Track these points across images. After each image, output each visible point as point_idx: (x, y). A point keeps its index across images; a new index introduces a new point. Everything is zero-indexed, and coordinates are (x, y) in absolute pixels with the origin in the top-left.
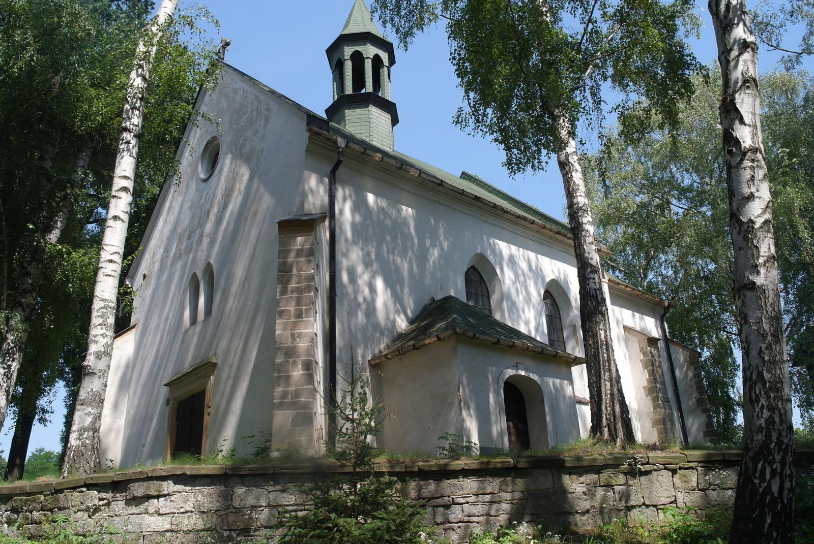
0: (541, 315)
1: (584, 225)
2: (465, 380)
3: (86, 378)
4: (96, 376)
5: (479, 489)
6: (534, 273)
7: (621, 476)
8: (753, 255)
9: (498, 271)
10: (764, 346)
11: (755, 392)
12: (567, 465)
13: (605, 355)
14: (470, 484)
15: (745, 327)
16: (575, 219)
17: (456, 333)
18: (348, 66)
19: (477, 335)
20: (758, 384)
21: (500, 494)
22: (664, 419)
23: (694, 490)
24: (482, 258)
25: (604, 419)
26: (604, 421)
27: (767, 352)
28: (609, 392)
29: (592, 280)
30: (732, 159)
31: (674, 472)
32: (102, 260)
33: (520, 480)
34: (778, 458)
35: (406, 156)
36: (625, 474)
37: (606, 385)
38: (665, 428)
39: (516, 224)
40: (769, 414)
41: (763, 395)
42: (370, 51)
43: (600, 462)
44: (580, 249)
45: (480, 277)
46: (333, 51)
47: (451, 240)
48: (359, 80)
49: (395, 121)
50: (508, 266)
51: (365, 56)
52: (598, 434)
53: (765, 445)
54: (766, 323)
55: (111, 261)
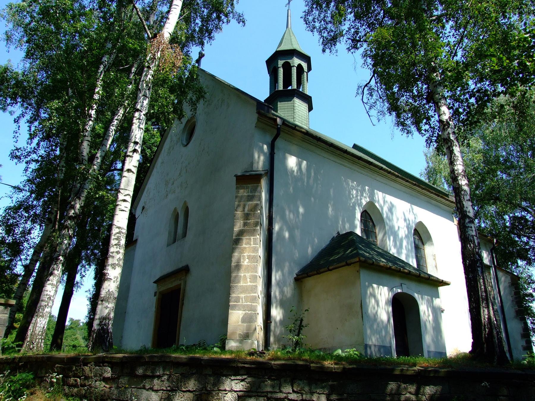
3: (106, 282)
4: (112, 281)
13: (483, 287)
18: (281, 71)
28: (486, 316)
32: (119, 199)
35: (317, 132)
37: (484, 311)
42: (296, 61)
46: (271, 63)
48: (287, 81)
49: (310, 108)
51: (292, 65)
55: (124, 201)
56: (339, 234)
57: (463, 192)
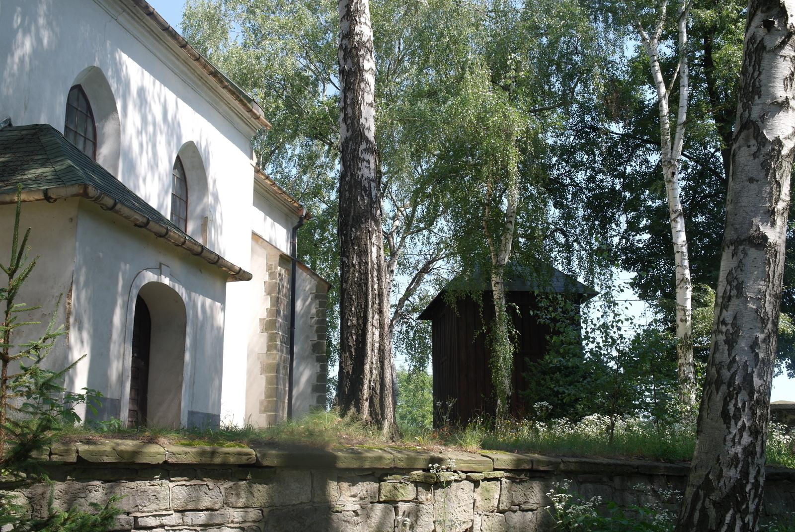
0: (167, 192)
1: (364, 73)
2: (82, 279)
5: (187, 502)
6: (169, 126)
7: (411, 487)
8: (771, 194)
9: (119, 106)
10: (761, 336)
11: (735, 405)
12: (341, 465)
13: (376, 287)
14: (173, 491)
15: (735, 302)
16: (352, 58)
17: (85, 194)
19: (119, 206)
20: (743, 392)
21: (222, 511)
22: (278, 365)
23: (492, 512)
24: (97, 76)
25: (366, 386)
26: (366, 392)
27: (763, 346)
28: (377, 345)
29: (365, 164)
30: (767, 38)
31: (476, 483)
33: (260, 487)
34: (752, 507)
36: (417, 484)
37: (373, 334)
38: (277, 377)
39: (158, 38)
40: (750, 439)
41: (746, 410)
43: (386, 464)
44: (353, 109)
45: (89, 103)
47: (57, 30)
50: (135, 106)
52: (353, 410)
53: (739, 486)
54: (770, 303)
56: (10, 125)
57: (362, 85)
